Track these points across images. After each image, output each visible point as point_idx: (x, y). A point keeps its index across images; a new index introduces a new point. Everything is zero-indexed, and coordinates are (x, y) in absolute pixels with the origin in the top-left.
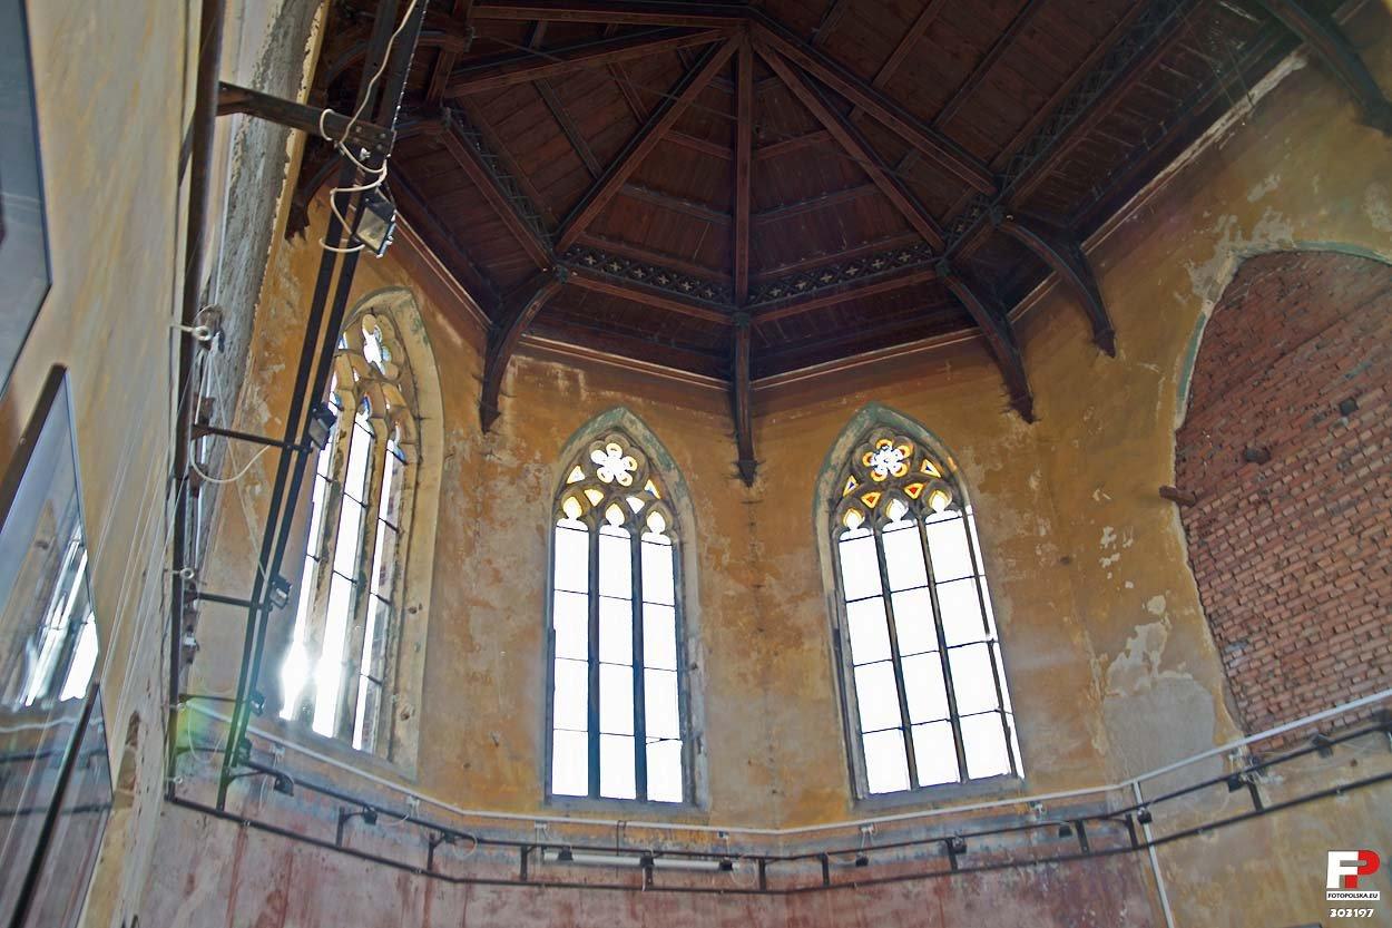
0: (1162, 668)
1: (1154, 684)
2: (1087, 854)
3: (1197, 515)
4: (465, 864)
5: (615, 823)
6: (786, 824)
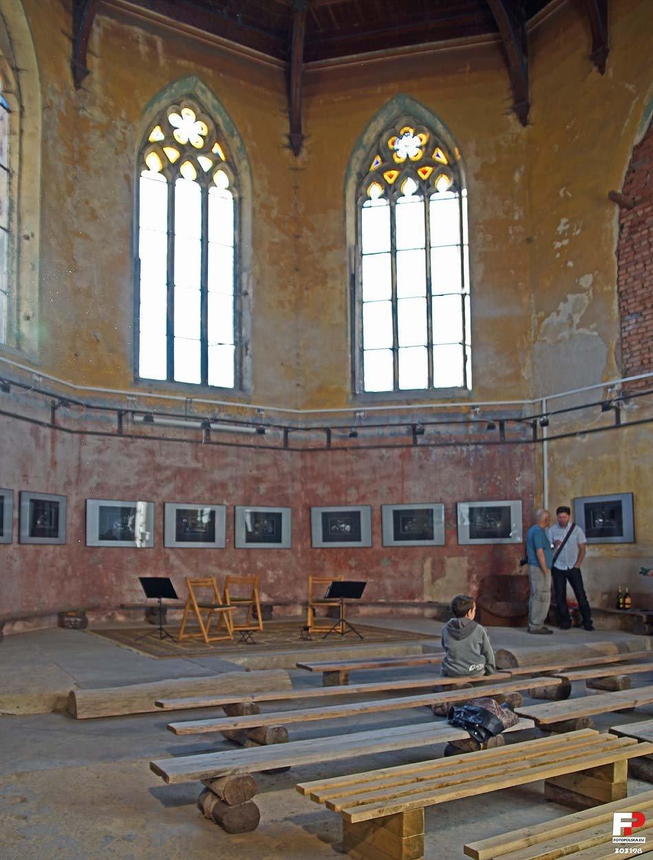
0: (578, 327)
1: (571, 336)
2: (503, 442)
3: (631, 217)
4: (79, 421)
5: (185, 399)
6: (304, 407)
